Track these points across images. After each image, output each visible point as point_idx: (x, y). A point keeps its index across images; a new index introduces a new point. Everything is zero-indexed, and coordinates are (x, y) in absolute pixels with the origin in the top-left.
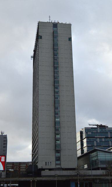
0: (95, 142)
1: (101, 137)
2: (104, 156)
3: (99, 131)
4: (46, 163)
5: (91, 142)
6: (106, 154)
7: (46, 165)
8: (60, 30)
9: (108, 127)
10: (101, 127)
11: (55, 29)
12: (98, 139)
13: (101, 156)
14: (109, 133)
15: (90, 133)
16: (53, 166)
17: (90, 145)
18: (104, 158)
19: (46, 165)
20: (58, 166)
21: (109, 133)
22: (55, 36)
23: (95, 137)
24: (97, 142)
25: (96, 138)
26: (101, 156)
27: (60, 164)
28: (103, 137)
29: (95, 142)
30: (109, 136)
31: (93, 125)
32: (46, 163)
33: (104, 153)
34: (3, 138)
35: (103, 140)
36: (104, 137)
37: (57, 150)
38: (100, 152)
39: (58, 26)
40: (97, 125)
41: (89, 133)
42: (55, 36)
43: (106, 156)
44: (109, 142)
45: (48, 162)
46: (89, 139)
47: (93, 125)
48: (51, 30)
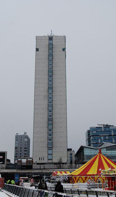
0: (99, 140)
1: (105, 135)
2: (90, 152)
3: (103, 130)
4: (40, 158)
5: (96, 139)
6: (92, 150)
7: (40, 160)
8: (54, 42)
9: (113, 126)
10: (107, 126)
11: (51, 41)
12: (102, 137)
13: (87, 152)
14: (112, 132)
15: (95, 132)
16: (46, 161)
17: (95, 143)
18: (90, 154)
19: (40, 160)
20: (50, 161)
21: (112, 132)
22: (51, 47)
23: (100, 135)
24: (101, 139)
25: (100, 136)
26: (87, 152)
27: (52, 159)
28: (106, 135)
29: (99, 140)
30: (113, 135)
31: (100, 125)
32: (40, 158)
33: (90, 150)
34: (24, 137)
35: (107, 138)
36: (108, 135)
37: (50, 147)
38: (86, 149)
39: (53, 38)
40: (104, 125)
41: (94, 132)
42: (51, 47)
43: (92, 152)
44: (112, 139)
45: (42, 158)
46: (94, 138)
47: (100, 125)
48: (47, 42)
